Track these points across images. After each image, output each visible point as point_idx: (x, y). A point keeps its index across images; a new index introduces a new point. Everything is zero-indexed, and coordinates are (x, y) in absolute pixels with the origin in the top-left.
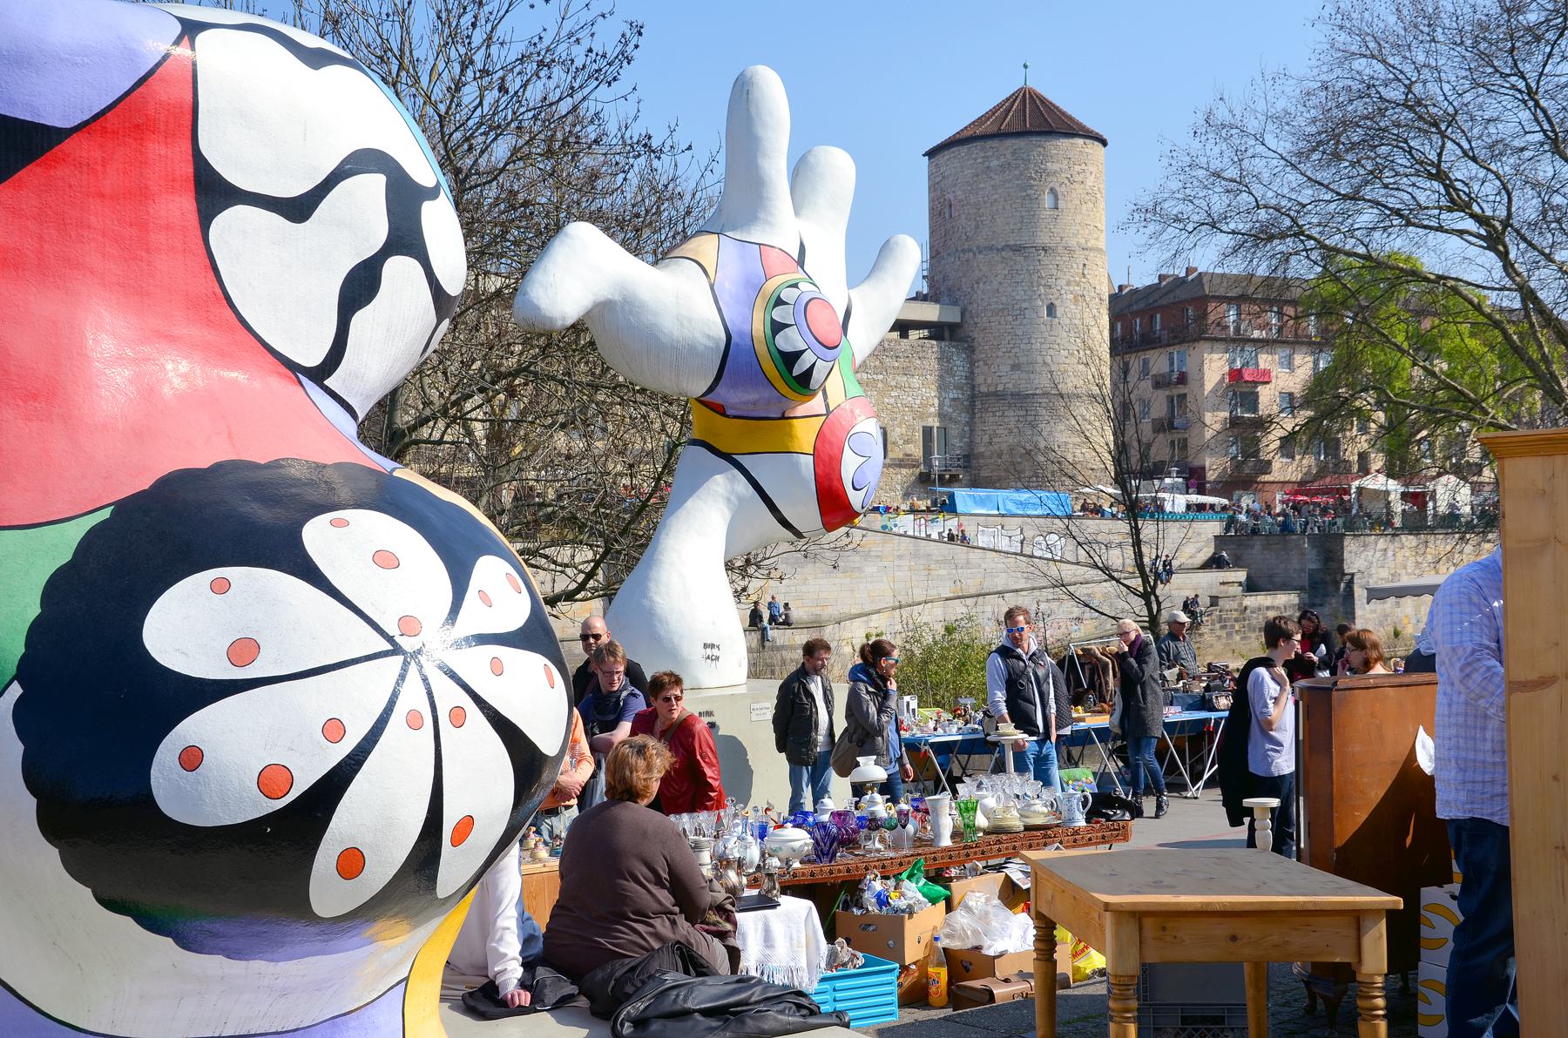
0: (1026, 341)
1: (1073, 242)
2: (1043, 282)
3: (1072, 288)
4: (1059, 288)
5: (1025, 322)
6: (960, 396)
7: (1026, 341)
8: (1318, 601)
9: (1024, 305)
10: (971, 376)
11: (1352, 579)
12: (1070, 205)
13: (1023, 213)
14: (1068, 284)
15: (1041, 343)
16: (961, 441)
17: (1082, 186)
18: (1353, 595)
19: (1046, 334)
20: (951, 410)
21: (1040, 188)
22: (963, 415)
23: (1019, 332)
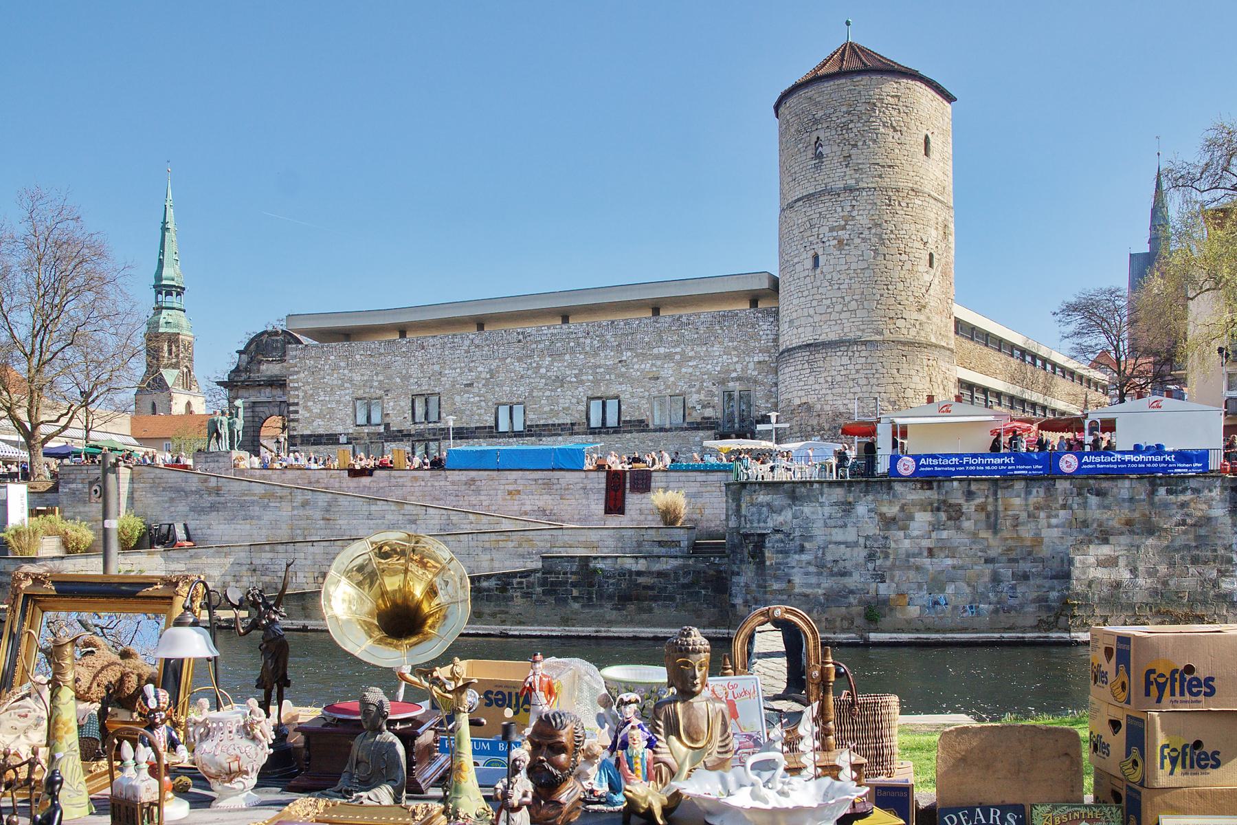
6: (767, 359)
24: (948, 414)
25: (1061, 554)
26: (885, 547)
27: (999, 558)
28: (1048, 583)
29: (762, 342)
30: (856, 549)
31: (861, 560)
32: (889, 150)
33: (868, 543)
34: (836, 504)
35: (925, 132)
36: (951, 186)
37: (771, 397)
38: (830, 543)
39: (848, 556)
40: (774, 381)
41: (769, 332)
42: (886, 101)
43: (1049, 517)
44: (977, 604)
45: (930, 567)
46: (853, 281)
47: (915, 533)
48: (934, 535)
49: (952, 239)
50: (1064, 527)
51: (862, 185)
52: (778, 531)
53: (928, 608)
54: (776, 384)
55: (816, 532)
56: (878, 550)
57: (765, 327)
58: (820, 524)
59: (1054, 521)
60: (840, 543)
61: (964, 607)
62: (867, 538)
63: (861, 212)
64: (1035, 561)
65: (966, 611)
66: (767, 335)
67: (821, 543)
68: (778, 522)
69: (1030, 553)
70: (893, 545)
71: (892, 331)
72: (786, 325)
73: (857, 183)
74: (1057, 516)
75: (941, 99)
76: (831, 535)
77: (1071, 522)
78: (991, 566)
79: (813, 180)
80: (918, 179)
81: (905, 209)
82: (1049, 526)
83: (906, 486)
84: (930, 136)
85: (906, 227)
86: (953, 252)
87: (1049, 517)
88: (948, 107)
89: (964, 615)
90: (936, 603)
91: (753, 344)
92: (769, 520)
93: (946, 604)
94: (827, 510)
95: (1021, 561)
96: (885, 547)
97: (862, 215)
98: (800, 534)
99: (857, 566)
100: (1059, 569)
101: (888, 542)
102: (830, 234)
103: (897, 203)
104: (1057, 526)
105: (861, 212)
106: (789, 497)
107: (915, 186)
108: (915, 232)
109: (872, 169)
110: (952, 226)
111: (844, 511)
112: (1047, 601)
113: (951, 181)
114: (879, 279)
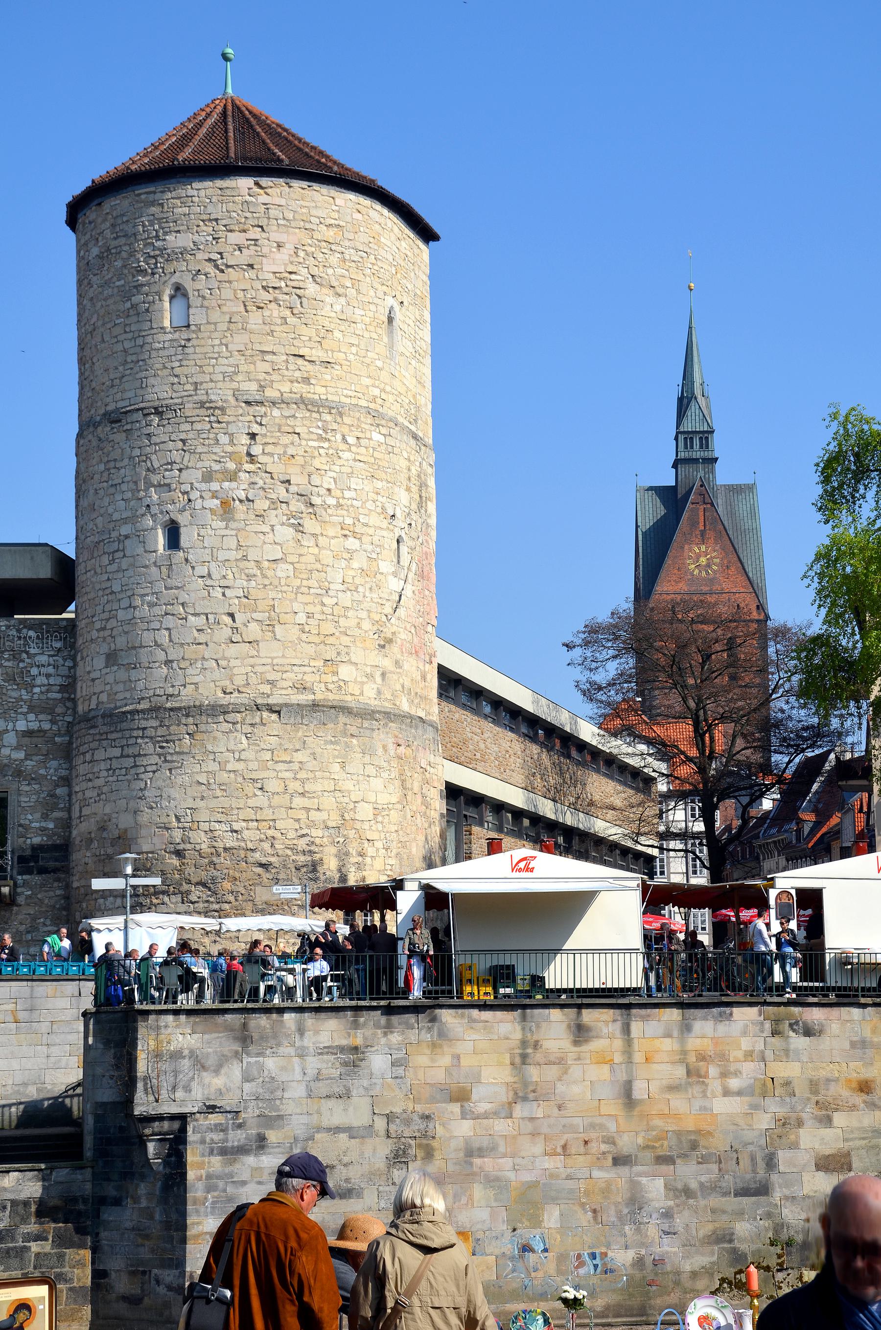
0: (125, 603)
1: (221, 393)
2: (155, 479)
3: (215, 486)
4: (184, 488)
5: (124, 564)
6: (46, 726)
7: (125, 603)
8: (110, 1190)
9: (125, 530)
10: (69, 687)
11: (183, 1130)
12: (215, 316)
13: (127, 345)
14: (208, 477)
15: (151, 605)
16: (45, 817)
17: (252, 274)
18: (184, 1175)
19: (160, 586)
20: (21, 755)
21: (155, 288)
22: (54, 764)
23: (116, 588)
24: (529, 874)
25: (751, 1148)
26: (425, 1136)
27: (640, 1155)
28: (732, 1203)
29: (37, 690)
30: (368, 1141)
31: (380, 1163)
32: (323, 333)
33: (393, 1128)
34: (328, 1050)
35: (390, 301)
36: (430, 406)
37: (54, 807)
38: (319, 1129)
39: (353, 1156)
40: (64, 773)
41: (51, 670)
42: (317, 235)
43: (724, 1075)
44: (604, 1250)
45: (511, 1175)
46: (253, 583)
47: (483, 1107)
48: (519, 1111)
49: (432, 507)
50: (752, 1094)
51: (270, 393)
52: (212, 1109)
53: (512, 1258)
54: (67, 781)
55: (288, 1108)
56: (413, 1142)
57: (43, 659)
58: (297, 1091)
59: (734, 1083)
60: (337, 1130)
61: (579, 1256)
62: (390, 1118)
63: (269, 449)
64: (703, 1160)
65: (582, 1264)
66: (48, 676)
67: (300, 1132)
68: (213, 1090)
69: (694, 1146)
70: (440, 1131)
71: (331, 686)
72: (99, 662)
73: (262, 388)
74: (737, 1073)
75: (412, 235)
76: (319, 1112)
77: (764, 1085)
78: (624, 1171)
79: (166, 372)
80: (376, 392)
81: (353, 449)
82: (727, 1093)
83: (463, 1016)
84: (397, 307)
85: (354, 483)
86: (434, 534)
87: (724, 1075)
88: (423, 251)
89: (582, 1271)
90: (526, 1248)
91: (15, 694)
92: (194, 1085)
93: (546, 1250)
94: (313, 1063)
95: (678, 1161)
96: (425, 1136)
97: (271, 455)
98: (257, 1112)
99: (371, 1176)
100: (748, 1176)
101: (431, 1126)
102: (204, 486)
103: (339, 437)
104: (739, 1093)
105: (269, 449)
106: (235, 1039)
107: (372, 406)
108: (372, 495)
109: (291, 367)
110: (431, 482)
111: (345, 1064)
112: (731, 1241)
113: (429, 396)
114: (305, 583)
